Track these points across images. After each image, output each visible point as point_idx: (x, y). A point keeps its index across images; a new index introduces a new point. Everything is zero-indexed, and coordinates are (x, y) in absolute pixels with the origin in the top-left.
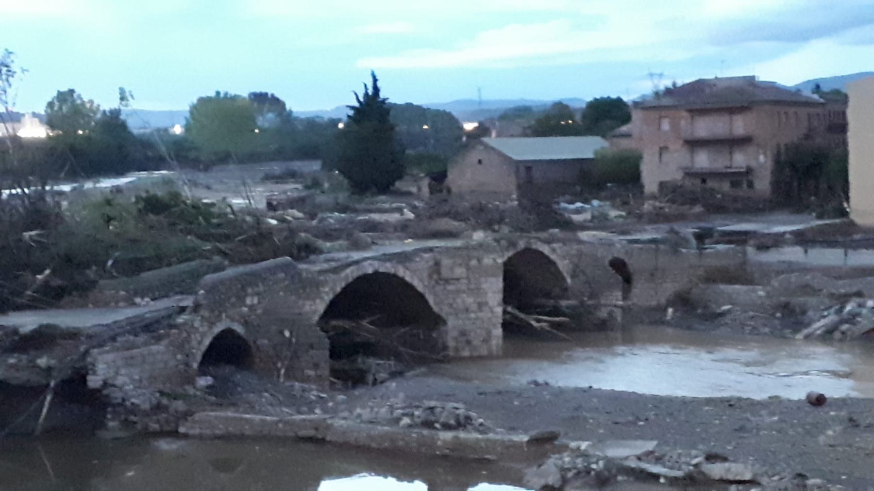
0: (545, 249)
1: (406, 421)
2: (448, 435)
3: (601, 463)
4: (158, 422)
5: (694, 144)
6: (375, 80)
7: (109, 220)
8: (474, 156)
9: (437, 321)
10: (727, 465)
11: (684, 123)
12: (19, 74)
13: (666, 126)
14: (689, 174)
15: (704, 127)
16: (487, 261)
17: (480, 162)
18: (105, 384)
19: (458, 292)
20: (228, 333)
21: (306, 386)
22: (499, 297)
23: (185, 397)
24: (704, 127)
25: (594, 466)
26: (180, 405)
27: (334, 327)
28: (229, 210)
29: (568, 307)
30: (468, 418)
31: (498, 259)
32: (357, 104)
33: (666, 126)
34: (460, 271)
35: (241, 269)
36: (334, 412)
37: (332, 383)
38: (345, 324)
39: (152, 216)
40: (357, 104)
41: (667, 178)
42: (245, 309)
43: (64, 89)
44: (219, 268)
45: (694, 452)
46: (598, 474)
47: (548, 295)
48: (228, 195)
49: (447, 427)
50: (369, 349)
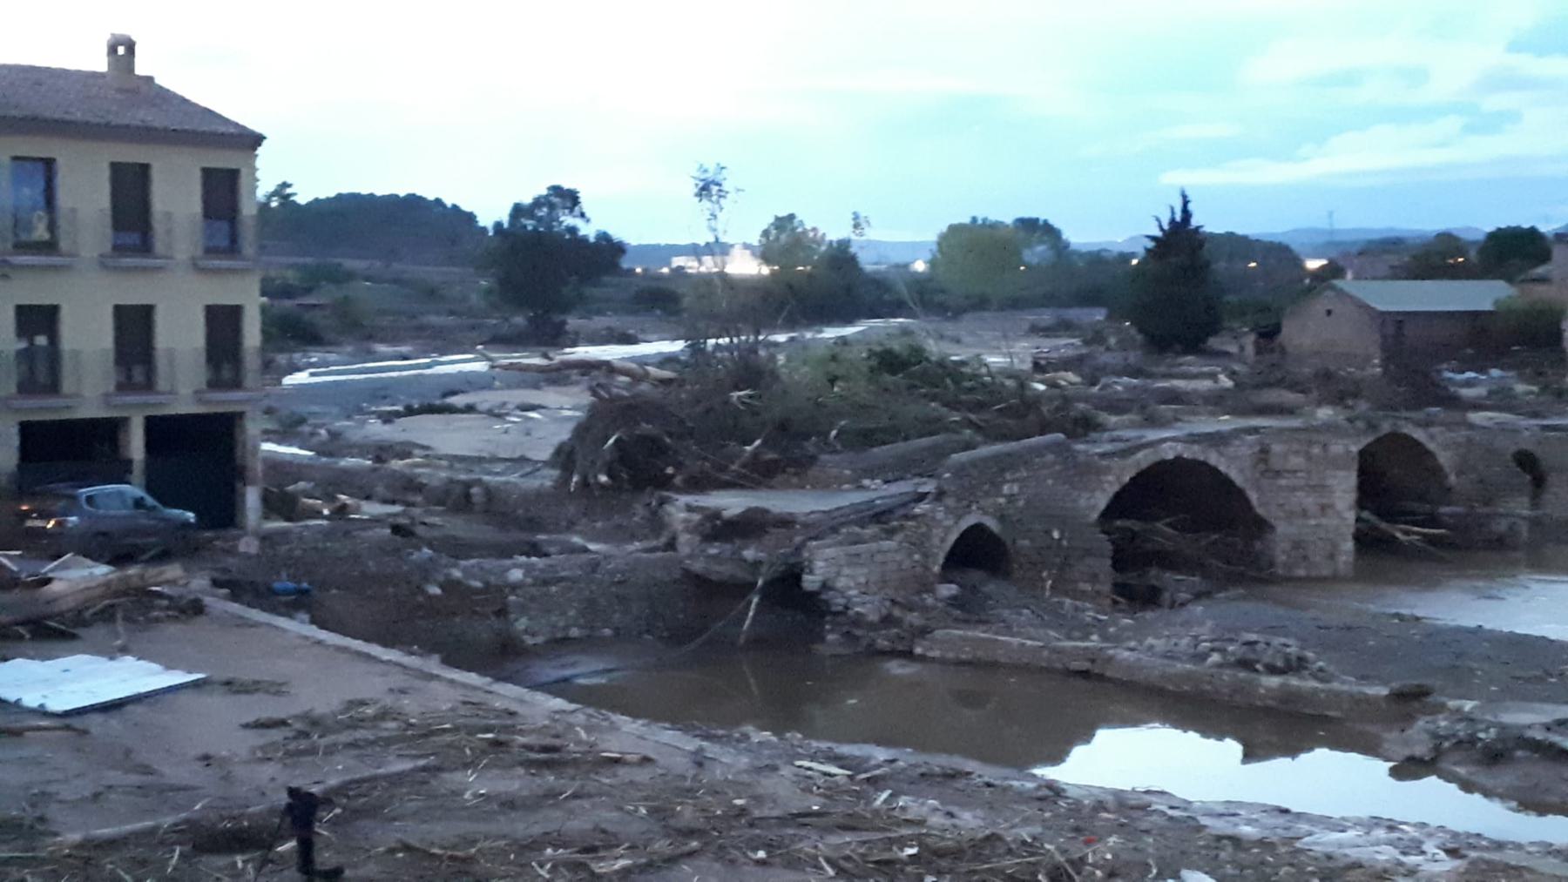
0: (1419, 434)
2: (1274, 681)
6: (1186, 202)
8: (1319, 305)
9: (1261, 526)
16: (1337, 448)
17: (1329, 312)
19: (1294, 489)
20: (978, 529)
22: (1352, 497)
25: (1482, 735)
29: (1451, 516)
30: (1301, 659)
34: (1296, 461)
37: (1115, 602)
38: (1134, 525)
39: (888, 378)
40: (1158, 233)
42: (1002, 500)
44: (968, 446)
48: (248, 210)
49: (1272, 670)
50: (1167, 561)
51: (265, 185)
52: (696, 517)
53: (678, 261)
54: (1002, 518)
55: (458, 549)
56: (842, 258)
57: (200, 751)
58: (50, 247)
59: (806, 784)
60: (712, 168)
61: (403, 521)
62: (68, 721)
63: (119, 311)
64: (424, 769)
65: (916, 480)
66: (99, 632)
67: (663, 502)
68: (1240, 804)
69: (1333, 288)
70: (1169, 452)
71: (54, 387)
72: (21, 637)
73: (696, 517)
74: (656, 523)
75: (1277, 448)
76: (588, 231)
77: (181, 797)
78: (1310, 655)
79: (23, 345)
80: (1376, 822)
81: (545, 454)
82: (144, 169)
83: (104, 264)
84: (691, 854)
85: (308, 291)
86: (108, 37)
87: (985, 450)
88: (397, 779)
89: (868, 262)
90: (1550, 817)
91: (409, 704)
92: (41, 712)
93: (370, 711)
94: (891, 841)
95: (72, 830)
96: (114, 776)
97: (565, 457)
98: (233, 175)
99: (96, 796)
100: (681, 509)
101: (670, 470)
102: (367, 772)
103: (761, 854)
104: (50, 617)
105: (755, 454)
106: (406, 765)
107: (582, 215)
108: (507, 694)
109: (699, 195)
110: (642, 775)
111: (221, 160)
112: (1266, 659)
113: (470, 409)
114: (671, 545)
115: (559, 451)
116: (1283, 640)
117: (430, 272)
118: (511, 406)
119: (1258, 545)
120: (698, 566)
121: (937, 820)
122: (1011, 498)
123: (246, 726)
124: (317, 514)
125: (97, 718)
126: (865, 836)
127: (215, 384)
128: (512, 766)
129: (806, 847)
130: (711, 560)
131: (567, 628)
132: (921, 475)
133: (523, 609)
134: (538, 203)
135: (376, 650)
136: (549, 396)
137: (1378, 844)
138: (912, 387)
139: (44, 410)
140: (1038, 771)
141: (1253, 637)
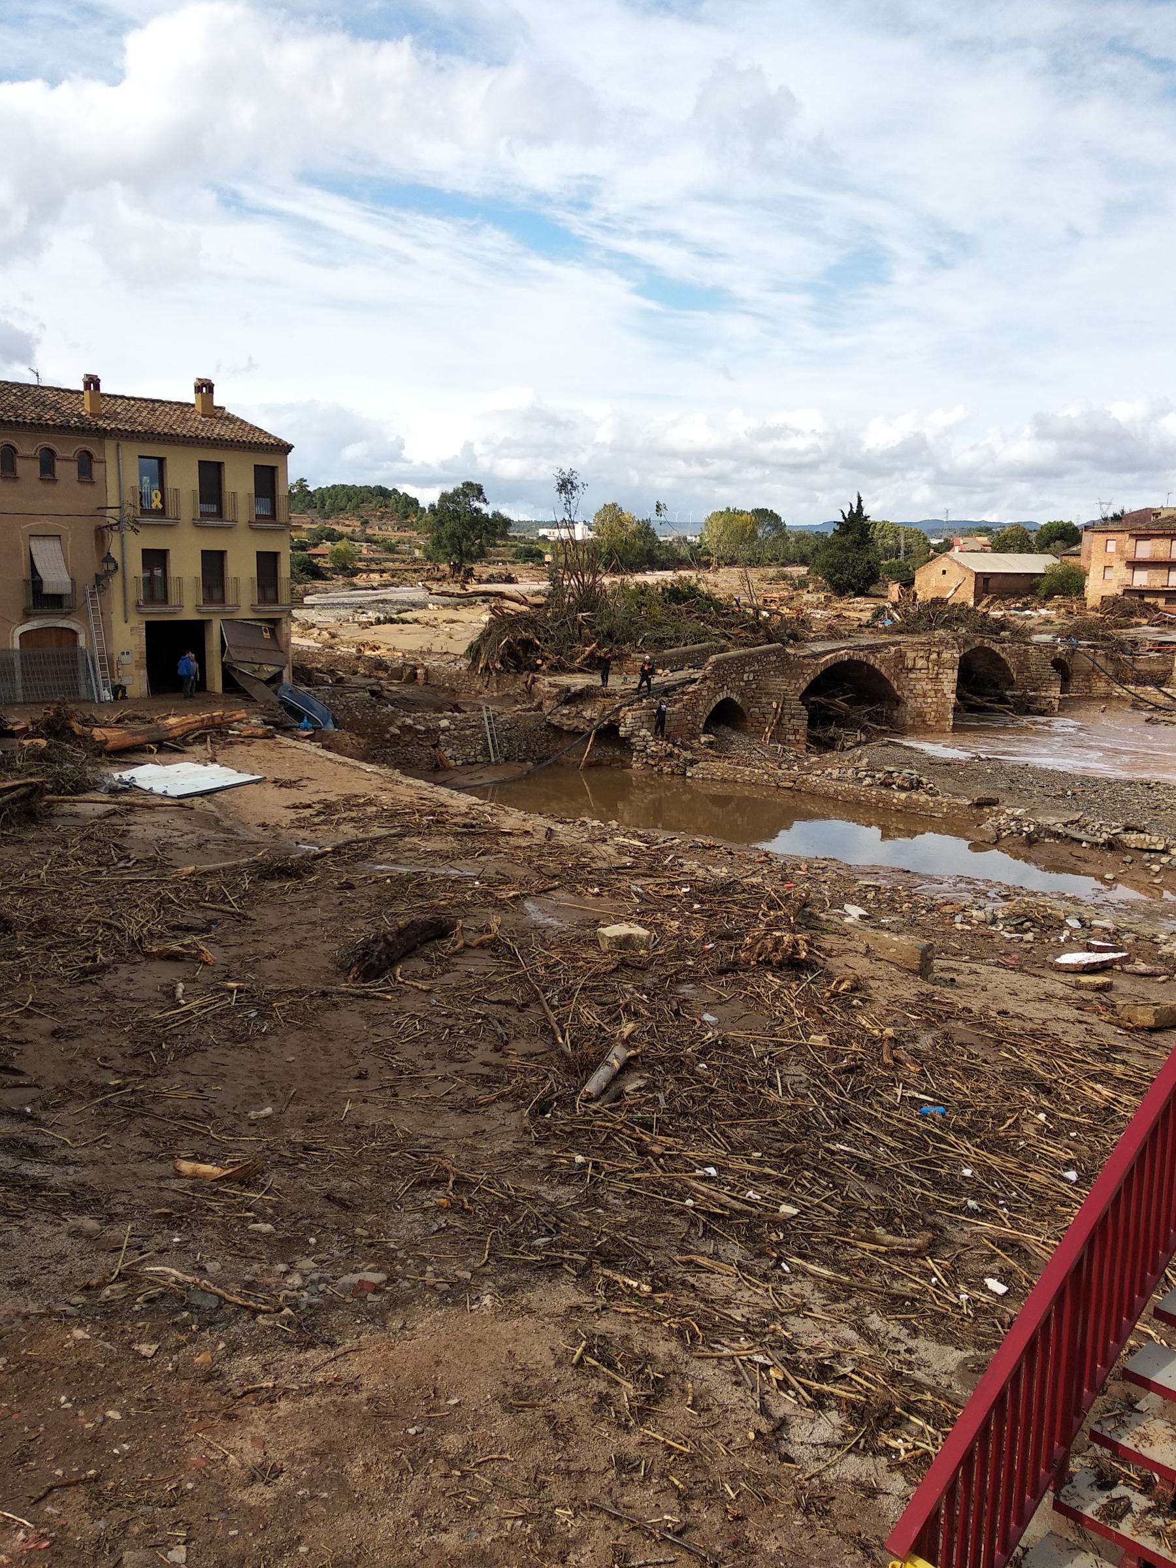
0: (997, 648)
1: (868, 781)
2: (903, 796)
3: (1032, 827)
4: (670, 766)
5: (1135, 565)
6: (860, 501)
7: (641, 605)
8: (942, 563)
9: (898, 701)
10: (1142, 836)
11: (1129, 544)
12: (581, 488)
13: (1112, 547)
14: (1128, 591)
15: (1145, 550)
16: (946, 655)
17: (944, 572)
18: (632, 734)
19: (918, 680)
20: (728, 701)
21: (787, 748)
22: (953, 686)
23: (692, 749)
24: (1145, 550)
25: (1026, 829)
26: (688, 755)
27: (813, 703)
28: (734, 603)
29: (1012, 697)
30: (919, 782)
31: (952, 655)
32: (842, 520)
33: (1112, 547)
34: (921, 663)
35: (742, 651)
36: (809, 770)
37: (808, 748)
38: (822, 700)
39: (674, 606)
40: (842, 520)
41: (1107, 593)
42: (742, 684)
43: (609, 503)
44: (723, 649)
45: (1114, 824)
46: (1029, 835)
47: (996, 686)
48: (282, 492)
49: (902, 788)
50: (842, 721)
51: (292, 478)
52: (556, 690)
53: (543, 532)
54: (742, 695)
55: (409, 705)
56: (645, 530)
57: (260, 821)
58: (162, 512)
59: (621, 850)
60: (567, 471)
61: (375, 688)
62: (181, 801)
63: (205, 553)
64: (394, 836)
65: (691, 671)
66: (198, 748)
67: (534, 680)
68: (881, 867)
69: (948, 557)
70: (844, 655)
71: (165, 601)
72: (151, 751)
73: (556, 690)
74: (529, 692)
75: (911, 654)
76: (487, 510)
77: (251, 848)
78: (924, 780)
79: (148, 574)
80: (961, 879)
81: (462, 648)
82: (219, 466)
83: (197, 525)
84: (554, 889)
85: (316, 545)
86: (195, 381)
87: (733, 653)
88: (377, 841)
89: (665, 536)
90: (1064, 874)
91: (385, 798)
92: (165, 796)
93: (362, 800)
94: (674, 884)
95: (187, 865)
96: (209, 833)
97: (474, 651)
98: (273, 470)
99: (200, 846)
100: (545, 683)
101: (539, 662)
102: (361, 836)
103: (596, 890)
104: (167, 740)
105: (592, 653)
106: (384, 832)
107: (485, 500)
108: (443, 794)
109: (560, 491)
110: (524, 842)
111: (266, 460)
112: (899, 781)
113: (416, 621)
114: (539, 707)
115: (471, 648)
116: (909, 771)
117: (391, 533)
118: (440, 621)
119: (895, 713)
120: (555, 721)
121: (701, 873)
122: (748, 682)
123: (288, 807)
124: (326, 683)
125: (199, 800)
126: (658, 881)
127: (263, 600)
128: (447, 834)
129: (623, 886)
130: (564, 716)
131: (475, 756)
132: (693, 667)
133: (449, 744)
134: (456, 493)
135: (364, 765)
136: (464, 614)
137: (961, 891)
138: (689, 612)
139: (160, 614)
140: (758, 846)
141: (891, 769)
